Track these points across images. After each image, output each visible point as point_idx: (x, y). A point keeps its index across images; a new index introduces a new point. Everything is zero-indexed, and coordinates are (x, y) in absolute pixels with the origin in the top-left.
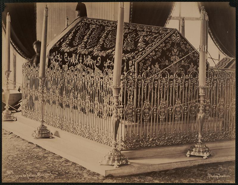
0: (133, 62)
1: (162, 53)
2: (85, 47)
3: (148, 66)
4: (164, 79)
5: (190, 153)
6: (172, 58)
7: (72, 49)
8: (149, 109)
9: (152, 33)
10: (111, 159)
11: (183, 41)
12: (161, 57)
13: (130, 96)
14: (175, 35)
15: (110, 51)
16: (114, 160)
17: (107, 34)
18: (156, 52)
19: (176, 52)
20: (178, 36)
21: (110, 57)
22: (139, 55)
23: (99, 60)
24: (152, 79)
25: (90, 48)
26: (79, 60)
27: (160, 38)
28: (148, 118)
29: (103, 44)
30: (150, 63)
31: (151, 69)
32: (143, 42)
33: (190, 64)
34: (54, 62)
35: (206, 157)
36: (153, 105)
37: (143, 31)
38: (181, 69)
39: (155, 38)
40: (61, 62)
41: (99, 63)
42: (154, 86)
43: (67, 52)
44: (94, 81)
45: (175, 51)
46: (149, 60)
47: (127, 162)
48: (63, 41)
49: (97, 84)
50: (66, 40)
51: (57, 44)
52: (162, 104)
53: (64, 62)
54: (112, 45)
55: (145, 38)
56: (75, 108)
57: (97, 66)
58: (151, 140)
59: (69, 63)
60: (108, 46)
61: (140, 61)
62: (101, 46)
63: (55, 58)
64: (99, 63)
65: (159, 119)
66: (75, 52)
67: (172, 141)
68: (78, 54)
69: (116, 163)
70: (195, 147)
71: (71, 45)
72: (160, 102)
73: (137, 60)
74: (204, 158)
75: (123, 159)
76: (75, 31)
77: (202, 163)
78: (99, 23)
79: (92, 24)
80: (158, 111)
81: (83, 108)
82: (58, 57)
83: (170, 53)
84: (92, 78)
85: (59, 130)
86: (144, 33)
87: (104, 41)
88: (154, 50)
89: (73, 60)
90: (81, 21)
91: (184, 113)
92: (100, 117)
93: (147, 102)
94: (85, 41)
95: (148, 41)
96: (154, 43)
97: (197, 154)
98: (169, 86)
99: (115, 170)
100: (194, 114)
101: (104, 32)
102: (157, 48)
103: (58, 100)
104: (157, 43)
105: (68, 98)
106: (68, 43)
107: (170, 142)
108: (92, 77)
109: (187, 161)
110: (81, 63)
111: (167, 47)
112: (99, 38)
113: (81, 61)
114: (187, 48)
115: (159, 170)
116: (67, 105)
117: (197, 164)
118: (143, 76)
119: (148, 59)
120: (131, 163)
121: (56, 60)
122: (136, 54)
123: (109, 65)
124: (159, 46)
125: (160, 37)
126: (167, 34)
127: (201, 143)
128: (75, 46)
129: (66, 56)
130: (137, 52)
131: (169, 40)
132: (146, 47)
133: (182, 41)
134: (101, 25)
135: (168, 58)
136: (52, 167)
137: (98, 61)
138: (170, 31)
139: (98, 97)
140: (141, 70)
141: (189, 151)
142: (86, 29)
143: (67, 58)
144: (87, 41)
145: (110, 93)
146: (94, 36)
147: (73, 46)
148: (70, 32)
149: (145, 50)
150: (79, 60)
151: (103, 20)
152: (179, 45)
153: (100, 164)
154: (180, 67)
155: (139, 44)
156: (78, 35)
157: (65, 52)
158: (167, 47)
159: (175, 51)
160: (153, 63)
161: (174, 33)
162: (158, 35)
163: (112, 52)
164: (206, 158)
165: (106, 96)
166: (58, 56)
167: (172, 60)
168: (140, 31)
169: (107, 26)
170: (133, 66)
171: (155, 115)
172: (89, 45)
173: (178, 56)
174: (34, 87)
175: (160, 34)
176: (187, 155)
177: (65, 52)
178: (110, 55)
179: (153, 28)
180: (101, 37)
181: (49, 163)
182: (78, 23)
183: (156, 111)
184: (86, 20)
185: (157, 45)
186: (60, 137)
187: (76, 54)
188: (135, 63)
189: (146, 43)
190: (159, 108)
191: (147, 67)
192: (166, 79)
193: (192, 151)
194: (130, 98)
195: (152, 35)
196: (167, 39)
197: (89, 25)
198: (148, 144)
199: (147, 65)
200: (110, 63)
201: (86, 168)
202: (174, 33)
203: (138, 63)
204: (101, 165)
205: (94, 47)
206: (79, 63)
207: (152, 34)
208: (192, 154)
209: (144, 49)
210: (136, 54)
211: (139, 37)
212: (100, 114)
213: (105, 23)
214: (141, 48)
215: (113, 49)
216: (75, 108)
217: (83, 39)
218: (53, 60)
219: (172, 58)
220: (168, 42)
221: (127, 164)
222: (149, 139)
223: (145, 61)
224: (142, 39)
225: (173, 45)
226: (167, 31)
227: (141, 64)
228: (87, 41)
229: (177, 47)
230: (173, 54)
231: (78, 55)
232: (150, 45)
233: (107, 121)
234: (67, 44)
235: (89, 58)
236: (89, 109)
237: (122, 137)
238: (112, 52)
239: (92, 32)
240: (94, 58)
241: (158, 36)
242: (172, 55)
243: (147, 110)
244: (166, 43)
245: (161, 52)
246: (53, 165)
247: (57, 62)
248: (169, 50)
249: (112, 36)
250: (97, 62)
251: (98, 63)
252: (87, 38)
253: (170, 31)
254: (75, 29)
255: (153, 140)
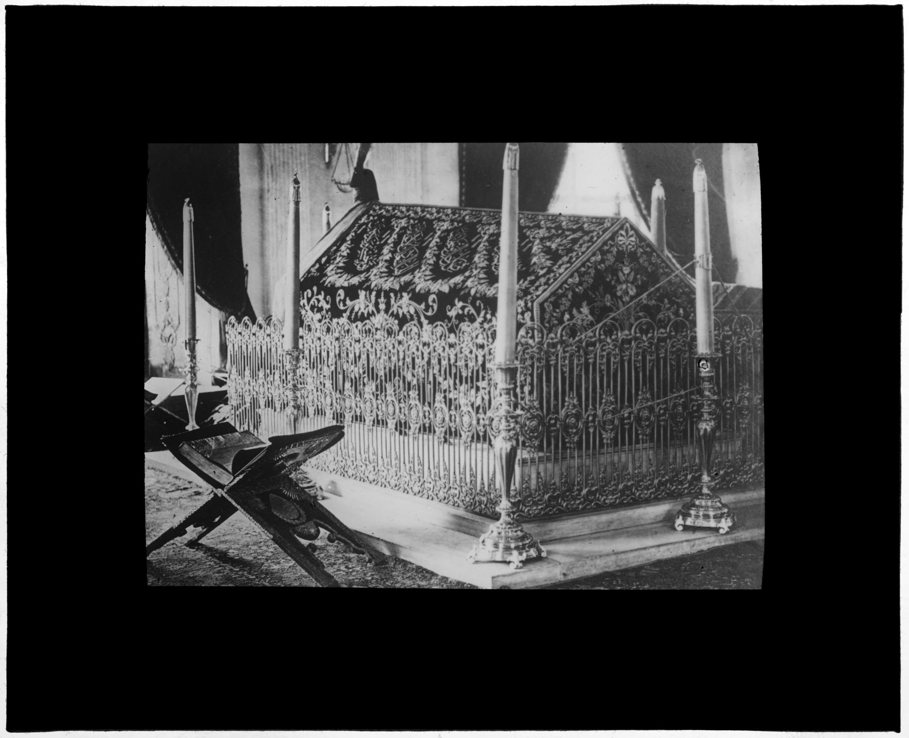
0: (526, 304)
1: (595, 278)
2: (390, 273)
3: (565, 311)
4: (609, 340)
5: (684, 520)
6: (618, 288)
7: (355, 280)
8: (578, 416)
9: (564, 230)
10: (501, 546)
11: (642, 247)
12: (594, 287)
13: (522, 387)
14: (623, 233)
15: (458, 279)
16: (507, 549)
17: (443, 239)
18: (581, 275)
19: (628, 274)
20: (632, 236)
21: (462, 293)
22: (540, 286)
23: (434, 301)
24: (543, 345)
25: (403, 275)
26: (377, 305)
27: (589, 241)
28: (576, 439)
29: (436, 264)
30: (568, 304)
31: (572, 317)
32: (542, 254)
33: (663, 302)
34: (310, 313)
35: (727, 529)
36: (587, 406)
37: (538, 227)
38: (641, 314)
39: (574, 241)
40: (327, 312)
41: (433, 310)
42: (586, 360)
43: (342, 287)
44: (429, 353)
45: (626, 272)
46: (567, 296)
47: (539, 551)
48: (328, 262)
49: (368, 355)
50: (335, 259)
51: (313, 270)
52: (606, 402)
53: (336, 313)
54: (461, 265)
55: (548, 244)
56: (379, 422)
57: (426, 317)
58: (584, 492)
59: (351, 312)
60: (451, 267)
61: (546, 300)
62: (430, 267)
63: (312, 302)
64: (433, 310)
65: (601, 439)
66: (365, 285)
67: (634, 494)
68: (372, 290)
69: (516, 557)
70: (694, 505)
71: (349, 269)
72: (601, 398)
73: (538, 296)
74: (721, 531)
75: (531, 546)
76: (354, 237)
77: (717, 544)
78: (416, 213)
79: (398, 218)
80: (599, 421)
81: (427, 425)
82: (319, 301)
83: (615, 278)
84: (426, 347)
85: (337, 478)
86: (542, 233)
87: (438, 256)
88: (577, 271)
89: (361, 304)
90: (366, 213)
91: (659, 421)
92: (401, 433)
93: (571, 400)
94: (387, 257)
95: (557, 250)
96: (575, 253)
97: (701, 523)
98: (622, 357)
99: (516, 573)
100: (681, 423)
101: (433, 236)
102: (583, 265)
103: (331, 405)
104: (583, 253)
105: (358, 399)
106: (341, 265)
107: (628, 496)
108: (400, 343)
109: (682, 542)
110: (382, 313)
111: (607, 263)
112: (423, 250)
113: (382, 306)
114: (653, 264)
115: (618, 568)
116: (424, 425)
117: (705, 547)
118: (559, 335)
119: (564, 295)
120: (549, 552)
121: (316, 309)
122: (532, 283)
123: (461, 312)
124: (588, 260)
125: (586, 238)
126: (604, 232)
127: (708, 495)
128: (361, 272)
129: (342, 298)
130: (533, 278)
131: (612, 246)
132: (554, 265)
133: (640, 247)
134: (421, 219)
135: (610, 289)
136: (347, 573)
137: (431, 304)
138: (612, 225)
139: (419, 390)
140: (549, 322)
141: (681, 517)
142: (383, 231)
143: (344, 301)
144: (392, 259)
145: (467, 383)
146: (408, 246)
147: (356, 273)
148: (342, 239)
149: (553, 272)
150: (377, 305)
151: (424, 208)
152: (633, 256)
153: (473, 560)
154: (638, 309)
155: (535, 260)
156: (365, 244)
157: (338, 288)
158: (607, 263)
159: (626, 272)
160: (576, 303)
161: (621, 228)
162: (579, 234)
163: (464, 282)
164: (727, 533)
165: (455, 389)
166: (321, 297)
167: (619, 294)
168: (529, 228)
169: (439, 220)
170: (529, 313)
171: (591, 430)
172: (399, 268)
173: (632, 283)
174: (247, 373)
175: (587, 233)
176: (676, 525)
177: (338, 288)
178: (461, 289)
179: (540, 217)
180: (427, 247)
181: (335, 564)
182: (359, 218)
183: (593, 421)
184: (380, 209)
185: (583, 258)
186: (343, 494)
187: (369, 289)
188: (532, 306)
189: (554, 256)
190: (599, 412)
191: (563, 314)
192: (613, 340)
193: (690, 515)
194: (522, 392)
195: (563, 235)
196: (605, 243)
197: (388, 220)
198: (579, 504)
199: (562, 308)
200: (463, 308)
201: (435, 571)
202: (621, 228)
203: (541, 305)
204: (477, 562)
205: (412, 271)
206: (378, 311)
207: (563, 232)
208: (689, 522)
209: (550, 270)
210: (532, 283)
211: (530, 242)
212: (401, 426)
213: (432, 214)
214: (542, 269)
215: (467, 274)
216: (378, 423)
217: (380, 254)
218: (308, 308)
219: (620, 289)
220: (608, 251)
221: (539, 559)
222: (580, 490)
223: (556, 299)
224: (540, 246)
225: (620, 256)
226: (603, 224)
227: (548, 307)
228: (392, 259)
229: (630, 263)
230: (622, 278)
231: (374, 293)
232: (565, 259)
233: (473, 452)
234: (339, 268)
235: (404, 299)
236: (397, 418)
237: (483, 484)
238: (464, 282)
239: (400, 236)
240: (419, 298)
241: (581, 237)
242: (618, 281)
243: (573, 420)
244: (604, 253)
245: (592, 275)
246: (347, 567)
247: (317, 312)
248: (614, 271)
249: (456, 244)
250: (427, 307)
251: (430, 310)
252: (390, 251)
253: (612, 225)
254: (355, 232)
255: (589, 493)
